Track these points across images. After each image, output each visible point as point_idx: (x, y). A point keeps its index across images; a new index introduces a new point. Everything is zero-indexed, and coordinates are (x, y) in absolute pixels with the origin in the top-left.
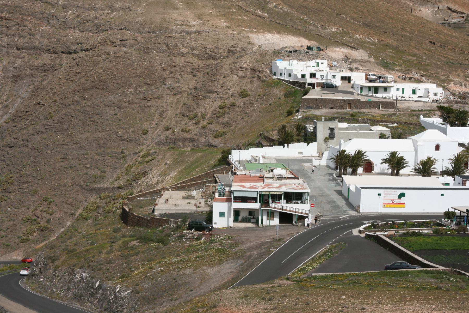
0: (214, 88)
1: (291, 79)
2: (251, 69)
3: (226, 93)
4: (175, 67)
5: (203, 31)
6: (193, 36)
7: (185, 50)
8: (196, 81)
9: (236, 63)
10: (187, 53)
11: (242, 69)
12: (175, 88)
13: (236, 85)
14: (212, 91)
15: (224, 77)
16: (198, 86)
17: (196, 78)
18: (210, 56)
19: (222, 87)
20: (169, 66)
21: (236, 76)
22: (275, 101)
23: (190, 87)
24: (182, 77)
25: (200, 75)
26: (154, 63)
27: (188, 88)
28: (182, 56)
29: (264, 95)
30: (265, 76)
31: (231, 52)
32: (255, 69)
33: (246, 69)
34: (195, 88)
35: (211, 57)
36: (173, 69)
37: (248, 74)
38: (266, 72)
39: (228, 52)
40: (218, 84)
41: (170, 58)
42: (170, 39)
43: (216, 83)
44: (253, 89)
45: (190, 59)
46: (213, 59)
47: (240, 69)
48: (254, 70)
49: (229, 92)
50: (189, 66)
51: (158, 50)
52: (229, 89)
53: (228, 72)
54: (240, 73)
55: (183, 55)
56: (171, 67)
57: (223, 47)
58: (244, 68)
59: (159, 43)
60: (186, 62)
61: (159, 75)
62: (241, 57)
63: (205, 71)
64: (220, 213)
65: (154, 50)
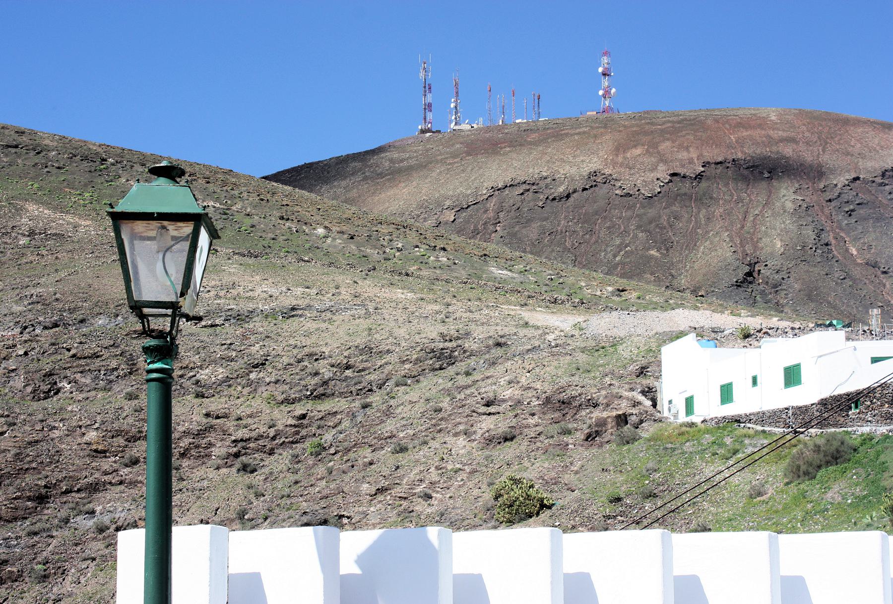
6: (258, 325)
11: (492, 409)
13: (464, 476)
21: (461, 441)
47: (483, 409)
54: (486, 425)
58: (504, 401)
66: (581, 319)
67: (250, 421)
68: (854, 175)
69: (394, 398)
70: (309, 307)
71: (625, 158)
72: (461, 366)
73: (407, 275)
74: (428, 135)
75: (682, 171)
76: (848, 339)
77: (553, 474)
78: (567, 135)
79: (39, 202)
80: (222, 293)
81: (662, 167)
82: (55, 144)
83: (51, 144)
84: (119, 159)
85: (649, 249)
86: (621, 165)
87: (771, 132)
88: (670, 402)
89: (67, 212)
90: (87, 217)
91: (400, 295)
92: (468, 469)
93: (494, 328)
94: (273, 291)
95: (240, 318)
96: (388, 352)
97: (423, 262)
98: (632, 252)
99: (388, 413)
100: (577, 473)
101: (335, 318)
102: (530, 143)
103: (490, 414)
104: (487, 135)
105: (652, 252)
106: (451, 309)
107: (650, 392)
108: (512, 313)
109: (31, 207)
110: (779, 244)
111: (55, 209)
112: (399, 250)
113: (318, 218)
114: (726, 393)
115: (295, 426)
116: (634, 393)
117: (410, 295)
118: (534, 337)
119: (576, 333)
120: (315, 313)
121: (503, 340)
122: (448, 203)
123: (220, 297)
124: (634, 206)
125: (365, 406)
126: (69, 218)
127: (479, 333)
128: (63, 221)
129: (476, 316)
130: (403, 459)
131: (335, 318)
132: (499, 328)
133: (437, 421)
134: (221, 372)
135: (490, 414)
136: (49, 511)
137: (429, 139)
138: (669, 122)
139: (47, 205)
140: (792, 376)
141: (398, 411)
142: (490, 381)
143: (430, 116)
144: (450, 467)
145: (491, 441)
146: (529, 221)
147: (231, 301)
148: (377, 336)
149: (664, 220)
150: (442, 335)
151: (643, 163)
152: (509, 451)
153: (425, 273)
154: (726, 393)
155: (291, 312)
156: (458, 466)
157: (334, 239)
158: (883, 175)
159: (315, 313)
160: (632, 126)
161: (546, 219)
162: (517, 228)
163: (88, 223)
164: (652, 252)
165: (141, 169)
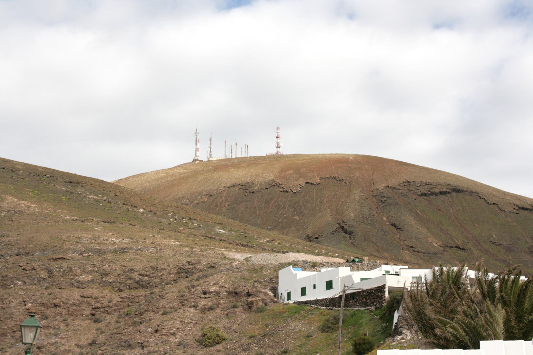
0: (137, 335)
1: (335, 292)
2: (229, 293)
3: (166, 342)
4: (56, 306)
5: (131, 248)
6: (109, 257)
7: (85, 278)
8: (97, 330)
9: (193, 286)
10: (89, 282)
11: (207, 296)
12: (44, 347)
13: (192, 325)
14: (131, 342)
15: (164, 314)
16: (102, 338)
17: (99, 325)
18: (137, 282)
19: (156, 331)
20: (43, 304)
21: (192, 310)
22: (298, 343)
23: (81, 343)
24: (67, 325)
25: (111, 319)
26: (10, 302)
27: (77, 345)
28: (78, 287)
29: (265, 336)
30: (263, 300)
31: (184, 272)
32: (237, 290)
33: (218, 293)
34: (93, 343)
35: (139, 285)
36: (50, 312)
37: (222, 301)
38: (266, 294)
39: (178, 273)
40: (147, 327)
41: (49, 291)
42: (59, 262)
43: (142, 327)
44: (234, 327)
45: (94, 291)
46: (143, 287)
47: (203, 296)
48: (236, 293)
49: (172, 339)
50: (89, 304)
51: (28, 281)
52: (174, 334)
53: (176, 304)
54: (202, 303)
55: (80, 285)
56: (48, 307)
57: (168, 266)
58: (212, 292)
59: (34, 269)
60: (83, 297)
61: (13, 324)
62: (206, 276)
63: (122, 311)
64: (305, 288)
65: (18, 279)
66: (249, 255)
67: (101, 299)
68: (386, 185)
69: (165, 290)
70: (131, 248)
71: (285, 175)
72: (195, 277)
73: (178, 232)
74: (197, 162)
75: (310, 181)
76: (351, 271)
77: (229, 325)
78: (259, 164)
79: (12, 195)
80: (93, 241)
81: (301, 179)
82: (22, 167)
83: (20, 167)
84: (52, 175)
85: (294, 216)
86: (283, 178)
87: (350, 165)
88: (282, 294)
89: (26, 200)
90: (35, 203)
91: (173, 243)
92: (194, 322)
93: (210, 259)
94: (115, 240)
95: (99, 252)
96: (164, 269)
97: (186, 225)
98: (286, 217)
99: (161, 297)
100: (239, 325)
101: (142, 253)
102: (243, 167)
103: (206, 298)
104: (224, 163)
105: (295, 217)
106: (194, 250)
107: (275, 290)
108: (220, 252)
109: (9, 198)
110: (352, 215)
111: (20, 198)
112: (176, 220)
113: (141, 204)
114: (303, 291)
115: (121, 302)
116: (267, 290)
117: (177, 243)
118: (227, 264)
119: (245, 263)
120: (134, 251)
121: (213, 265)
122: (204, 193)
123: (92, 243)
124: (288, 196)
125: (152, 293)
126: (26, 203)
127: (204, 262)
128: (24, 204)
129: (204, 253)
130: (166, 318)
131: (142, 253)
132: (213, 259)
133: (183, 302)
134: (90, 277)
135: (206, 298)
136: (7, 340)
137: (197, 163)
138: (305, 159)
139: (16, 197)
140: (329, 285)
141: (166, 296)
142: (207, 283)
143: (198, 153)
144: (186, 321)
145: (204, 310)
146: (241, 202)
147: (97, 245)
148: (160, 262)
149: (301, 203)
150: (189, 262)
151: (293, 177)
152: (210, 316)
153: (186, 231)
154: (303, 291)
155: (123, 251)
156: (190, 321)
157: (147, 214)
158: (399, 185)
159: (134, 251)
160: (289, 161)
161: (248, 201)
162: (235, 205)
163: (35, 205)
164: (295, 217)
165: (61, 180)
